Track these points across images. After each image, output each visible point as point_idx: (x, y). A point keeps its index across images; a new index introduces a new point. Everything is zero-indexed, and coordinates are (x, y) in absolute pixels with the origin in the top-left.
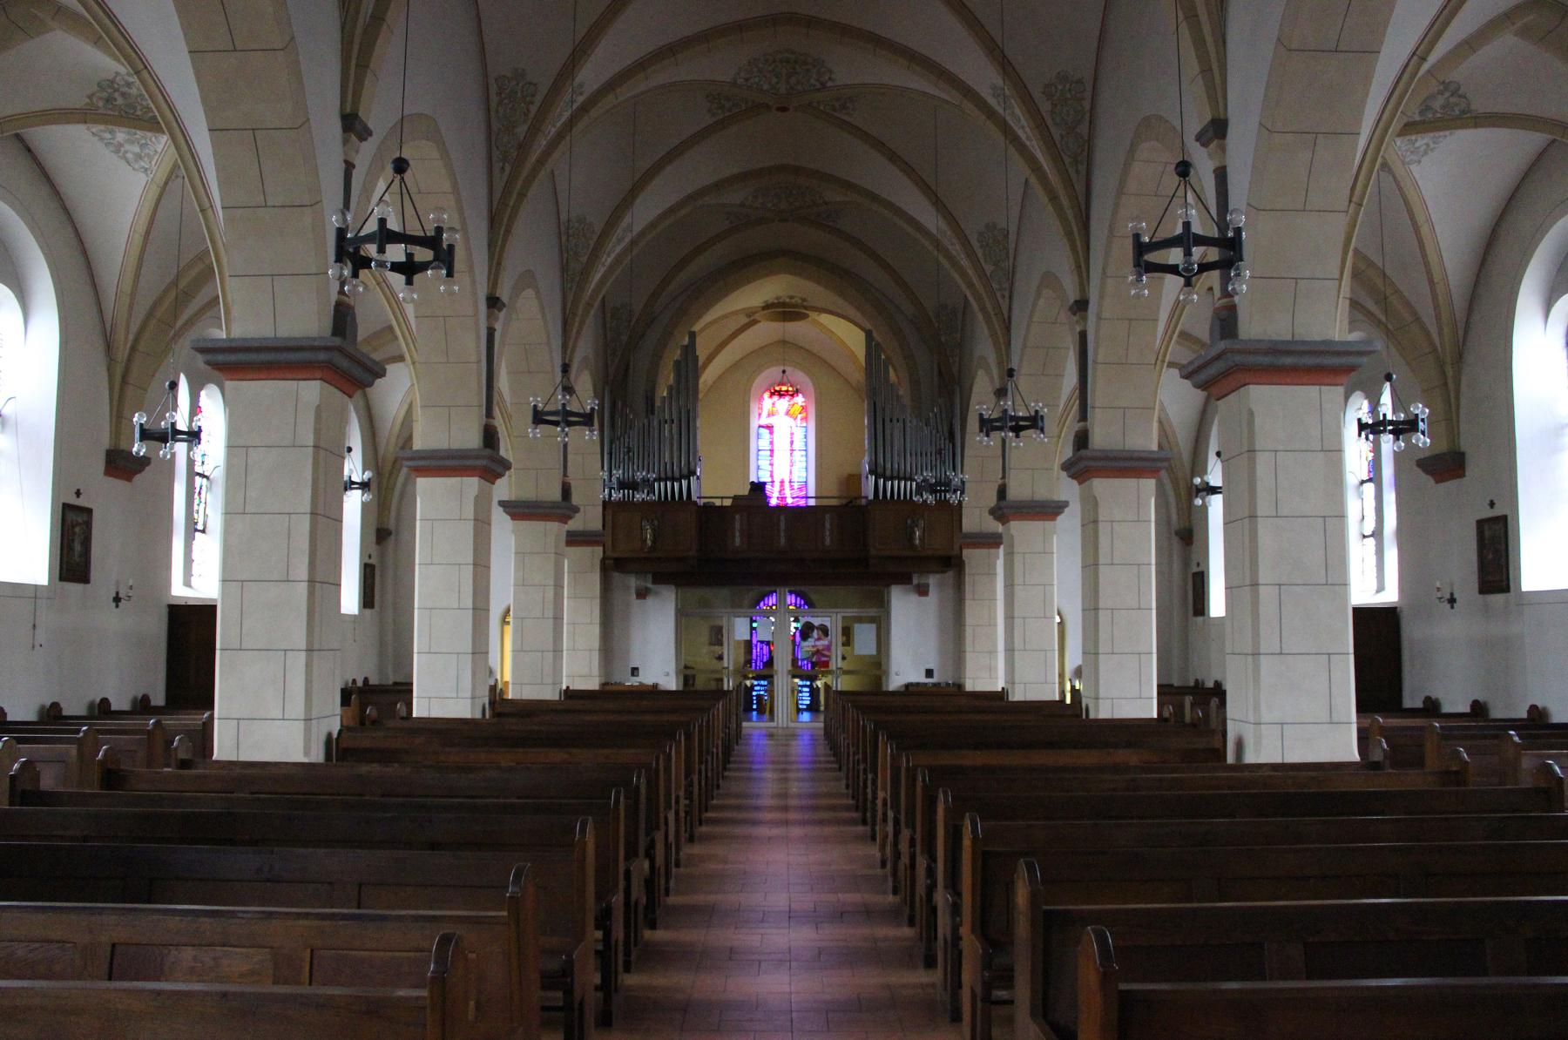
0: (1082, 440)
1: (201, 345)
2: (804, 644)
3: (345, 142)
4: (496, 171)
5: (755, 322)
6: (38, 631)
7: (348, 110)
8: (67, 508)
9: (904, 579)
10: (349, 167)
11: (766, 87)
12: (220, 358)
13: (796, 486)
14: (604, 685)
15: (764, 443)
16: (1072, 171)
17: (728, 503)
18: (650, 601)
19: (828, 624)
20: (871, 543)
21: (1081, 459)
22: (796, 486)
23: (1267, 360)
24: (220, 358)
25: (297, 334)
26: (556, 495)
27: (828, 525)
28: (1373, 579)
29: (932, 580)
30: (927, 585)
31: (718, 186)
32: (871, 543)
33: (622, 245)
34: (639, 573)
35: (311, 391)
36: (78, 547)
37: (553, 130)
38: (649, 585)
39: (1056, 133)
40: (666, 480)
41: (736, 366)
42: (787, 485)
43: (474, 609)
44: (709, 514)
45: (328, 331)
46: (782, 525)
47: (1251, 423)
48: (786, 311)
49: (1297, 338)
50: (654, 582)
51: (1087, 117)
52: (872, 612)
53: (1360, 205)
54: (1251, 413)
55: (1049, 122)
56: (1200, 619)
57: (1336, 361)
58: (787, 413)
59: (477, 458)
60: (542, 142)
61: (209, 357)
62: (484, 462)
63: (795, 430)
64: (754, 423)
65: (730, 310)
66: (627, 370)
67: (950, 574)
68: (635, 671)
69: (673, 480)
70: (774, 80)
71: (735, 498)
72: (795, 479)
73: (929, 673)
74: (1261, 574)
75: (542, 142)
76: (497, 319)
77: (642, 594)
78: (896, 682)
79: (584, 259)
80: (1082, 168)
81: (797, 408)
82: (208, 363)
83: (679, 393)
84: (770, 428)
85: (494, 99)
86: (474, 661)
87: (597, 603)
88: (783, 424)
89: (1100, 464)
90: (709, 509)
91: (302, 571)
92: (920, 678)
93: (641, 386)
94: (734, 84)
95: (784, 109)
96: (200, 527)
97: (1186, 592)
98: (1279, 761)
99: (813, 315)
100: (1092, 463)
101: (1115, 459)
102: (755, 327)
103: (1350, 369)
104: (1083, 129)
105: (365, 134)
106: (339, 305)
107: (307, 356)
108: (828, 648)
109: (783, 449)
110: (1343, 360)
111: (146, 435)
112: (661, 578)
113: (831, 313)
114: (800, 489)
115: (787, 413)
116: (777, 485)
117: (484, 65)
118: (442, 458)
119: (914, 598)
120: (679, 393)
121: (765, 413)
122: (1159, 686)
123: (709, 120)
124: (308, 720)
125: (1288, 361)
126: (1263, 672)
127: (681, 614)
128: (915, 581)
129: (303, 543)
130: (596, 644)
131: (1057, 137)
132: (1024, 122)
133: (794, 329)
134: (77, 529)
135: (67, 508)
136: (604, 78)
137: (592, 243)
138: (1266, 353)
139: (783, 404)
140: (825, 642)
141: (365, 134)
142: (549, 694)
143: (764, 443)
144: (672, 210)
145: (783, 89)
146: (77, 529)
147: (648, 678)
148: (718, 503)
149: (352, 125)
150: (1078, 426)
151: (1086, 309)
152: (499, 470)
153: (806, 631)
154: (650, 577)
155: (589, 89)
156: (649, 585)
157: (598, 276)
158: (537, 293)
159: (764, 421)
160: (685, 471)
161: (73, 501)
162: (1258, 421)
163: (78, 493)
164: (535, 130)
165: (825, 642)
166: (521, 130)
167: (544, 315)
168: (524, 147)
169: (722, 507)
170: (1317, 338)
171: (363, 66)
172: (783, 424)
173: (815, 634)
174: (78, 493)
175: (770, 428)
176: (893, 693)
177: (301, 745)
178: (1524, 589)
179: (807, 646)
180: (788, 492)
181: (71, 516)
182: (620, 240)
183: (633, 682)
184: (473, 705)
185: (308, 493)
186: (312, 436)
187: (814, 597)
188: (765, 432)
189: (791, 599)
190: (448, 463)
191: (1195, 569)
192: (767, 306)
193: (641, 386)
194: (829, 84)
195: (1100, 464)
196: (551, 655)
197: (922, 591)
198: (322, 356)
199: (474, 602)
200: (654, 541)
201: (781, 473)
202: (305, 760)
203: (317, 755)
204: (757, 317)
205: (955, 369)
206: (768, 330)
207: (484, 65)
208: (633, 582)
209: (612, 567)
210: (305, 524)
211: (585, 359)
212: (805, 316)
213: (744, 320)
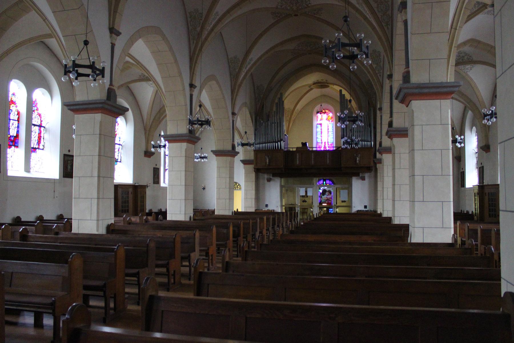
0: (390, 124)
1: (66, 104)
2: (323, 197)
3: (111, 37)
4: (192, 43)
5: (312, 89)
6: (56, 192)
7: (111, 26)
8: (65, 155)
9: (357, 175)
10: (113, 46)
11: (289, 8)
12: (72, 107)
13: (330, 144)
14: (256, 210)
15: (319, 130)
16: (386, 28)
17: (295, 150)
18: (272, 183)
19: (332, 191)
20: (351, 162)
21: (391, 131)
22: (330, 144)
23: (416, 91)
24: (72, 107)
25: (94, 99)
26: (230, 148)
27: (328, 157)
28: (124, 174)
29: (367, 175)
30: (364, 177)
31: (282, 43)
32: (351, 162)
33: (250, 65)
34: (268, 173)
35: (98, 117)
36: (69, 167)
37: (209, 28)
38: (271, 177)
39: (379, 15)
40: (273, 142)
41: (307, 105)
42: (327, 143)
43: (185, 185)
44: (289, 154)
45: (105, 98)
46: (313, 157)
47: (413, 116)
48: (322, 85)
49: (431, 82)
50: (273, 176)
51: (390, 8)
52: (346, 186)
53: (456, 29)
54: (413, 111)
55: (376, 11)
56: (463, 188)
57: (445, 90)
58: (327, 119)
59: (186, 136)
60: (206, 33)
61: (69, 107)
62: (187, 138)
63: (329, 125)
64: (315, 123)
65: (300, 85)
66: (263, 107)
67: (373, 173)
68: (267, 206)
69: (275, 142)
70: (291, 5)
71: (297, 148)
72: (329, 141)
73: (365, 207)
74: (416, 171)
75: (206, 33)
76: (193, 91)
77: (269, 180)
78: (354, 210)
79: (237, 70)
80: (390, 27)
81: (330, 117)
82: (69, 109)
83: (277, 113)
84: (321, 124)
85: (189, 19)
86: (185, 202)
87: (254, 183)
88: (325, 123)
89: (395, 133)
90: (288, 152)
91: (96, 174)
92: (363, 209)
93: (267, 112)
94: (277, 8)
95: (296, 15)
96: (119, 160)
97: (459, 179)
98: (422, 242)
99: (331, 86)
100: (393, 133)
101: (401, 131)
102: (311, 92)
103: (452, 93)
104: (389, 12)
105: (118, 34)
106: (109, 89)
107: (96, 106)
108: (331, 198)
109: (324, 132)
110: (448, 89)
111: (154, 147)
112: (275, 175)
113: (336, 85)
114: (331, 145)
115: (327, 119)
116: (323, 143)
117: (185, 9)
118: (176, 137)
119: (360, 181)
120: (277, 113)
121: (319, 119)
122: (455, 214)
123: (273, 21)
124: (98, 220)
125: (426, 91)
126: (416, 208)
127: (281, 187)
128: (361, 176)
129: (96, 164)
130: (254, 197)
131: (380, 16)
132: (368, 12)
133: (325, 91)
134: (69, 162)
135: (65, 155)
136: (225, 10)
137: (239, 65)
138: (417, 88)
139: (325, 116)
140: (330, 196)
141: (118, 34)
142: (228, 213)
143: (319, 130)
144: (267, 52)
145: (295, 8)
146: (69, 162)
147: (271, 208)
148: (291, 150)
149: (113, 31)
150: (389, 119)
151: (392, 78)
152: (195, 140)
153: (324, 191)
154: (271, 175)
155: (221, 13)
156: (271, 177)
157: (242, 76)
158: (218, 83)
159: (319, 122)
160: (279, 139)
161: (67, 153)
162: (415, 114)
163: (69, 151)
164: (202, 28)
165: (330, 196)
166: (199, 29)
167: (221, 90)
168: (200, 34)
169: (293, 151)
170: (439, 82)
171: (115, 12)
172: (325, 123)
173: (327, 193)
174: (69, 151)
175: (321, 124)
176: (354, 214)
177: (95, 228)
178: (9, 175)
179: (324, 197)
180: (327, 146)
181: (66, 158)
182: (249, 63)
183: (266, 209)
184: (185, 216)
185: (97, 149)
186: (98, 131)
187: (335, 181)
188: (319, 126)
189: (328, 182)
190: (177, 138)
191: (462, 171)
192: (314, 84)
193: (267, 112)
194: (310, 5)
195: (395, 133)
196: (228, 201)
197: (363, 179)
198: (100, 106)
199: (185, 183)
200: (269, 163)
201: (325, 140)
202: (97, 233)
203: (103, 231)
204: (312, 87)
205: (374, 102)
206: (316, 92)
207: (185, 9)
208: (266, 176)
209: (258, 171)
210: (97, 158)
211: (245, 104)
212: (328, 86)
213: (308, 89)
